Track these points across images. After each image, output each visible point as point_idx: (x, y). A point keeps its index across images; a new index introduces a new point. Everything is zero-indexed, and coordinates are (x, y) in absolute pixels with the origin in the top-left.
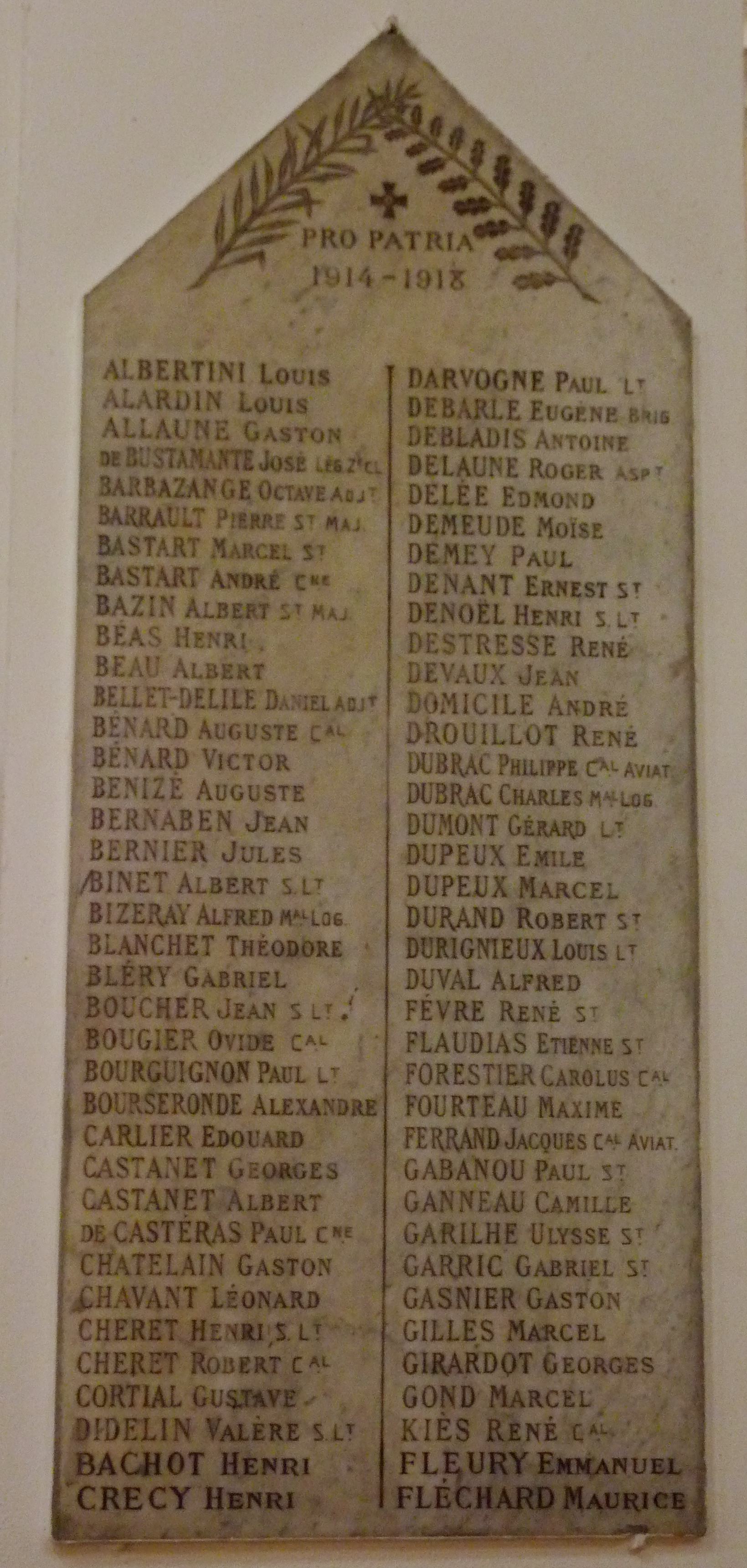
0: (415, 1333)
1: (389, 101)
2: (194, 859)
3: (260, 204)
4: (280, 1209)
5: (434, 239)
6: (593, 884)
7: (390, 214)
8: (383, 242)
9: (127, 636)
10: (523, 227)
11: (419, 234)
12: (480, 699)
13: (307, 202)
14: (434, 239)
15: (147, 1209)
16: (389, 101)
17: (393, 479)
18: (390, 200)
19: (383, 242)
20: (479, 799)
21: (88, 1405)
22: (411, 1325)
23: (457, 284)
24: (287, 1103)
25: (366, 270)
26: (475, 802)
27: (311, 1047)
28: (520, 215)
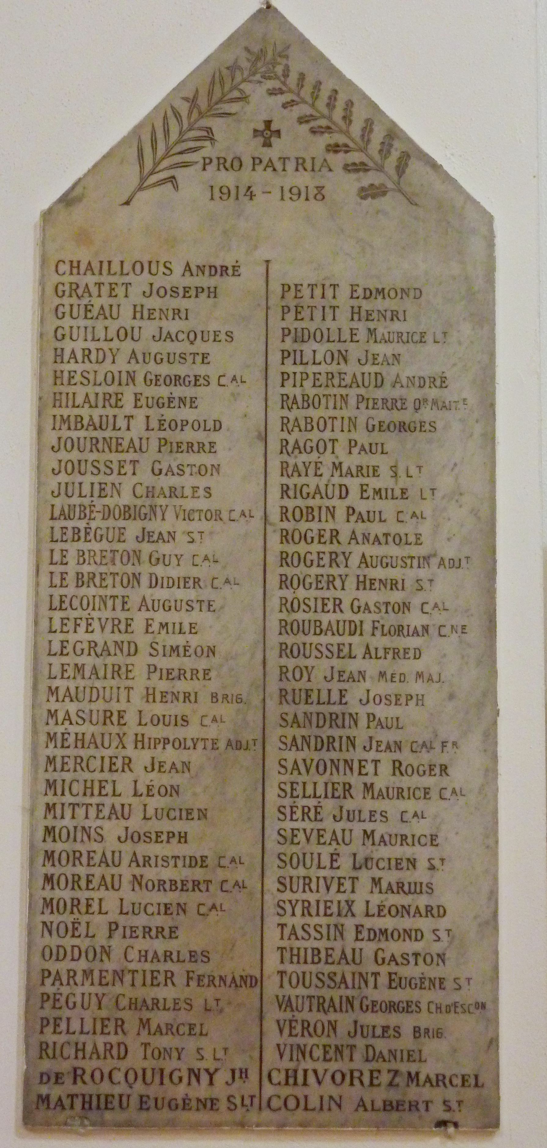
0: (83, 650)
1: (265, 60)
2: (209, 986)
3: (181, 135)
4: (184, 297)
5: (300, 164)
6: (425, 789)
7: (267, 144)
8: (262, 167)
9: (95, 312)
10: (380, 169)
11: (289, 158)
12: (149, 906)
13: (209, 136)
14: (300, 164)
15: (74, 678)
16: (265, 60)
17: (264, 373)
18: (268, 133)
19: (262, 167)
20: (304, 669)
21: (360, 868)
22: (79, 644)
23: (319, 197)
24: (176, 1002)
25: (249, 188)
26: (306, 667)
27: (227, 587)
28: (375, 158)
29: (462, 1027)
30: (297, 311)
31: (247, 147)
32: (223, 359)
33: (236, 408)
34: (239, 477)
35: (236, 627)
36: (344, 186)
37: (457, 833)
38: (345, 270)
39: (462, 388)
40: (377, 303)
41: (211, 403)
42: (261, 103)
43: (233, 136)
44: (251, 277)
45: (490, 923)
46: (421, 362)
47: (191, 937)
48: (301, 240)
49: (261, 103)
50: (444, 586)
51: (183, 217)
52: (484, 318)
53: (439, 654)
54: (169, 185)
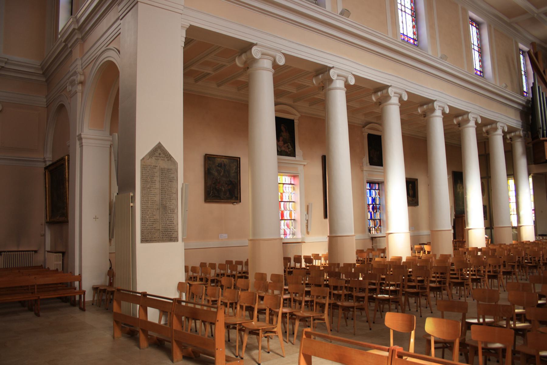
18: (160, 154)
29: (175, 233)
30: (162, 170)
31: (158, 155)
32: (156, 174)
33: (157, 179)
34: (158, 185)
35: (157, 198)
36: (166, 159)
37: (542, 212)
38: (166, 167)
39: (175, 178)
40: (169, 170)
41: (155, 178)
42: (159, 151)
43: (157, 154)
44: (158, 167)
45: (178, 224)
46: (172, 175)
47: (154, 226)
48: (162, 164)
49: (159, 151)
50: (174, 195)
51: (153, 161)
52: (177, 172)
53: (174, 201)
54: (61, 254)
